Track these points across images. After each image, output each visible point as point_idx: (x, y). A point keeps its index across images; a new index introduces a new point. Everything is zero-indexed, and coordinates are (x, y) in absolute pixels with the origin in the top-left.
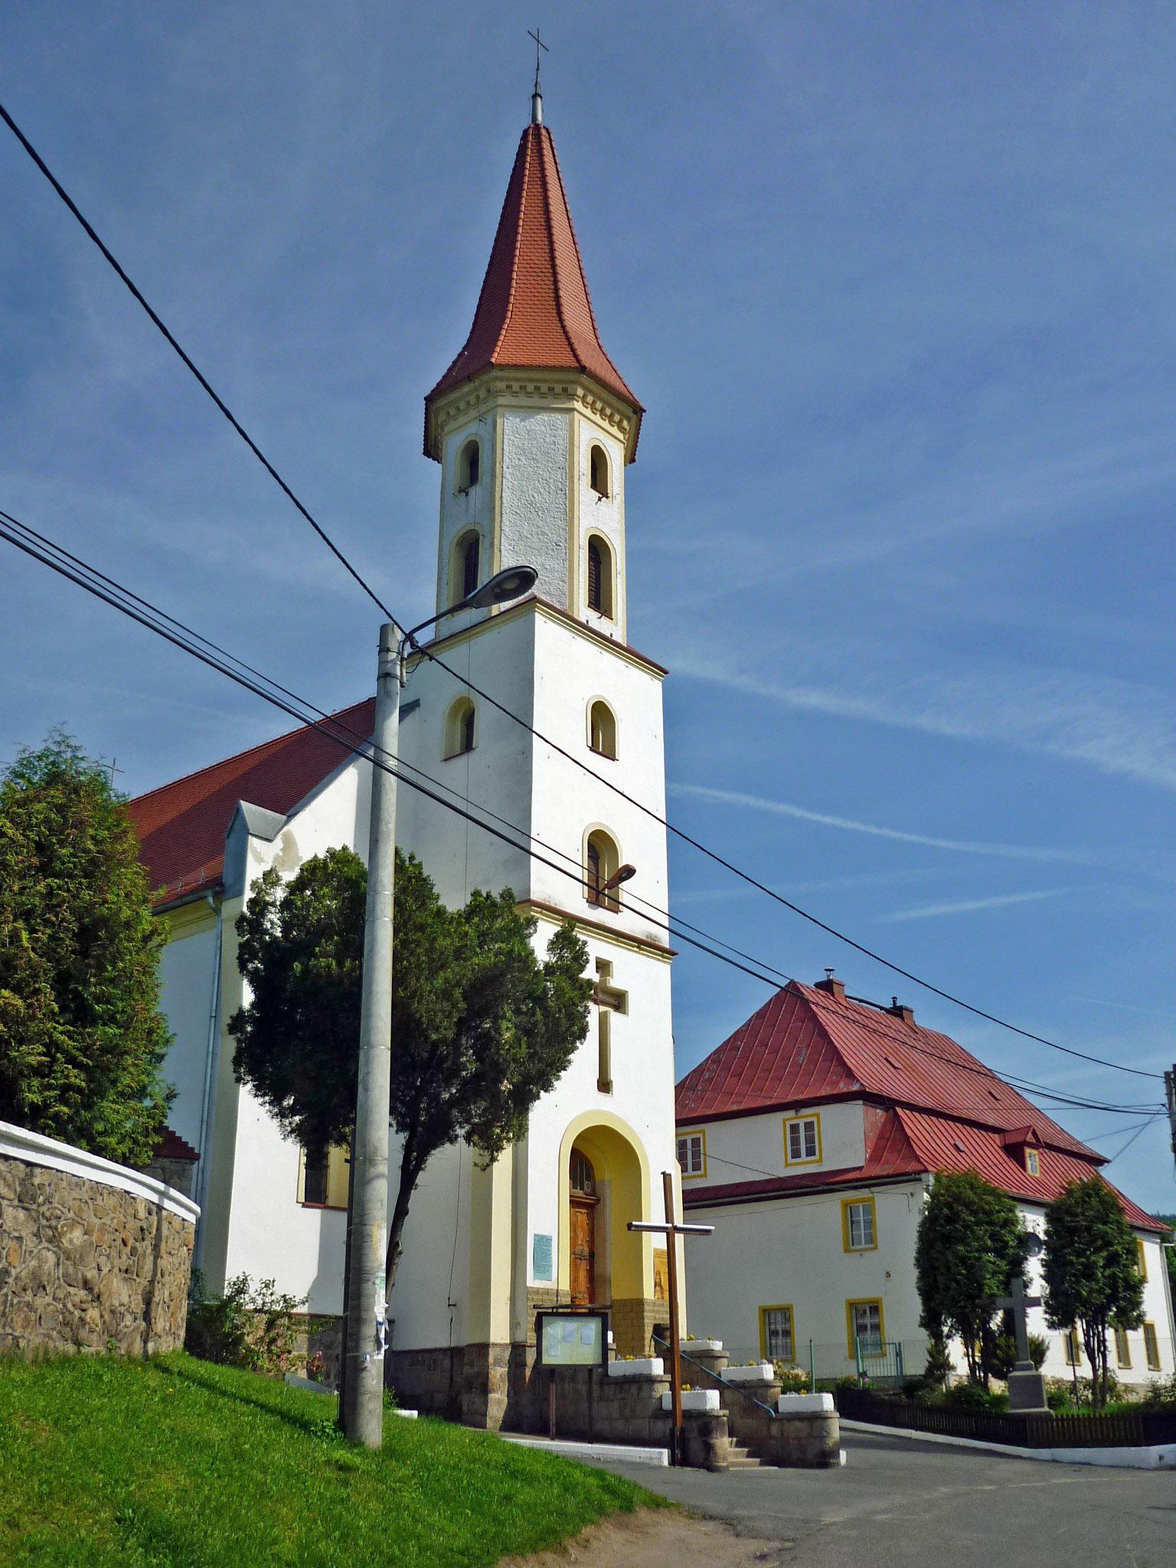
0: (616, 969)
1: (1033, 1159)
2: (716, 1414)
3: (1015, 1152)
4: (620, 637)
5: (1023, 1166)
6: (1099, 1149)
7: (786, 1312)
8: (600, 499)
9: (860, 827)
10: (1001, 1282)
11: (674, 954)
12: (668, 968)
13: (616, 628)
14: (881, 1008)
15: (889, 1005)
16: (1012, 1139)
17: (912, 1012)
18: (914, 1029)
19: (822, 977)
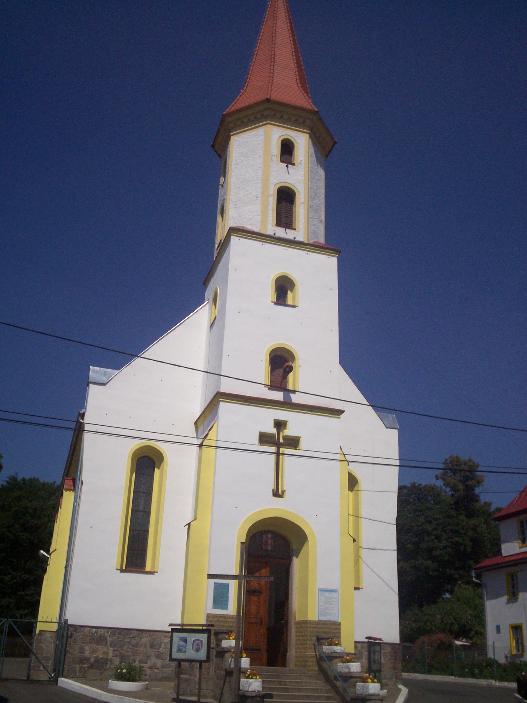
8: (287, 166)
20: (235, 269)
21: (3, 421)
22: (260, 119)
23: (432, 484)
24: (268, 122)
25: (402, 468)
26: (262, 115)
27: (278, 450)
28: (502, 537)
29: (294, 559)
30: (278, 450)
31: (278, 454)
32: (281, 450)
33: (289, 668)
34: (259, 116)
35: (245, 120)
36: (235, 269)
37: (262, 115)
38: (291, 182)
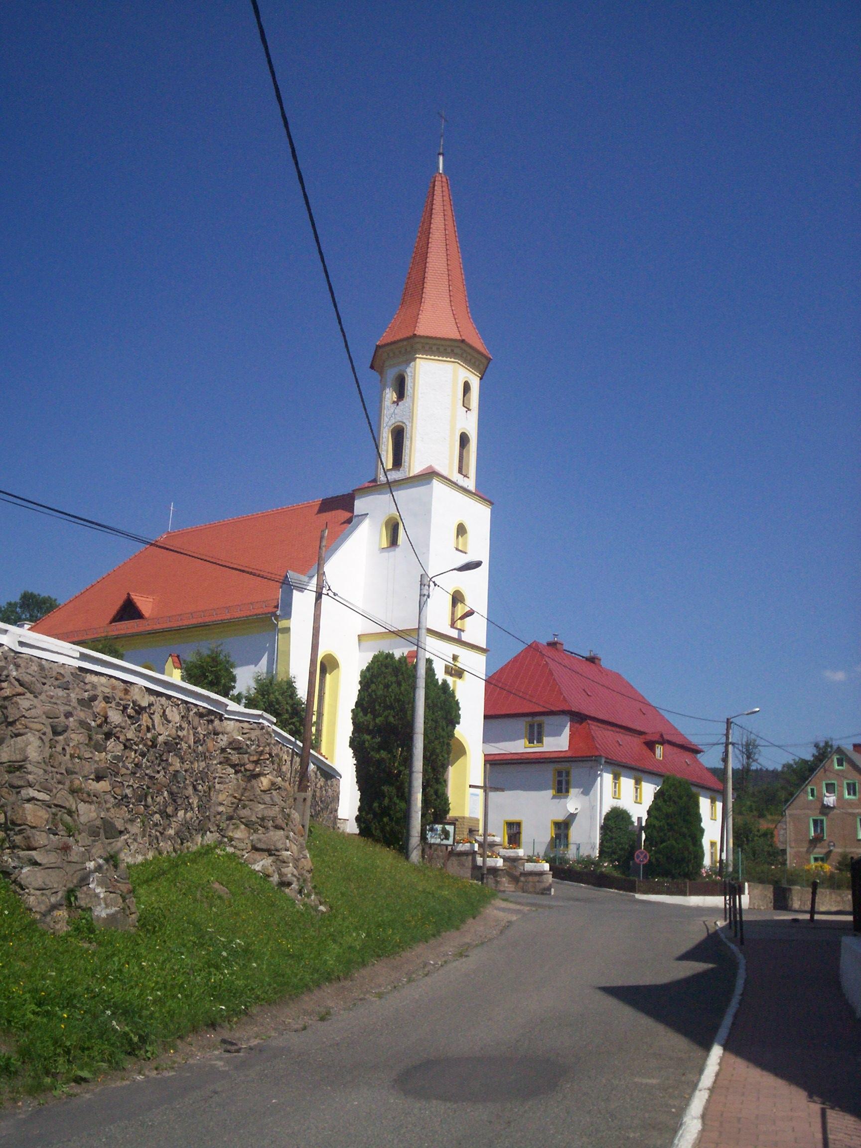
0: (459, 659)
1: (659, 750)
2: (500, 868)
3: (650, 745)
4: (472, 488)
5: (654, 754)
6: (695, 740)
7: (518, 824)
8: (467, 412)
9: (698, 1103)
10: (162, 1049)
11: (488, 651)
12: (484, 658)
13: (470, 484)
14: (583, 657)
15: (587, 654)
16: (649, 738)
17: (600, 660)
18: (602, 671)
19: (551, 639)
20: (793, 1131)
21: (124, 530)
22: (449, 353)
23: (30, 592)
24: (457, 361)
25: (495, 723)
26: (452, 351)
27: (812, 917)
28: (728, 1055)
29: (450, 766)
30: (812, 917)
31: (812, 912)
32: (807, 917)
33: (294, 870)
34: (449, 350)
35: (434, 348)
36: (793, 1131)
37: (452, 351)
38: (468, 429)
